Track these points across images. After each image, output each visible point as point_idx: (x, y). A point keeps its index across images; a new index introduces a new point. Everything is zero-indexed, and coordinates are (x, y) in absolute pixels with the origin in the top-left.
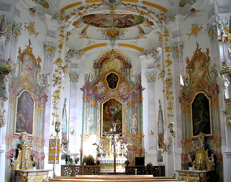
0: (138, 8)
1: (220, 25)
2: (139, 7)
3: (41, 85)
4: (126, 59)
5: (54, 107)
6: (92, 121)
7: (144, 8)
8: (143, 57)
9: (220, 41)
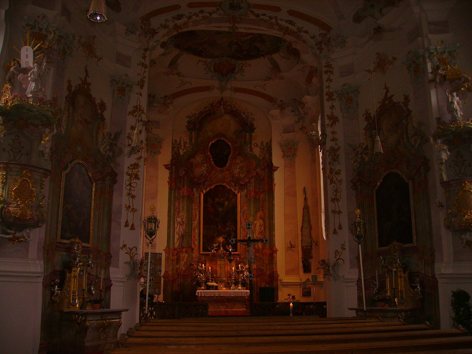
0: (279, 22)
1: (432, 53)
3: (106, 152)
4: (244, 116)
5: (129, 194)
6: (184, 225)
7: (291, 23)
8: (276, 112)
9: (433, 81)
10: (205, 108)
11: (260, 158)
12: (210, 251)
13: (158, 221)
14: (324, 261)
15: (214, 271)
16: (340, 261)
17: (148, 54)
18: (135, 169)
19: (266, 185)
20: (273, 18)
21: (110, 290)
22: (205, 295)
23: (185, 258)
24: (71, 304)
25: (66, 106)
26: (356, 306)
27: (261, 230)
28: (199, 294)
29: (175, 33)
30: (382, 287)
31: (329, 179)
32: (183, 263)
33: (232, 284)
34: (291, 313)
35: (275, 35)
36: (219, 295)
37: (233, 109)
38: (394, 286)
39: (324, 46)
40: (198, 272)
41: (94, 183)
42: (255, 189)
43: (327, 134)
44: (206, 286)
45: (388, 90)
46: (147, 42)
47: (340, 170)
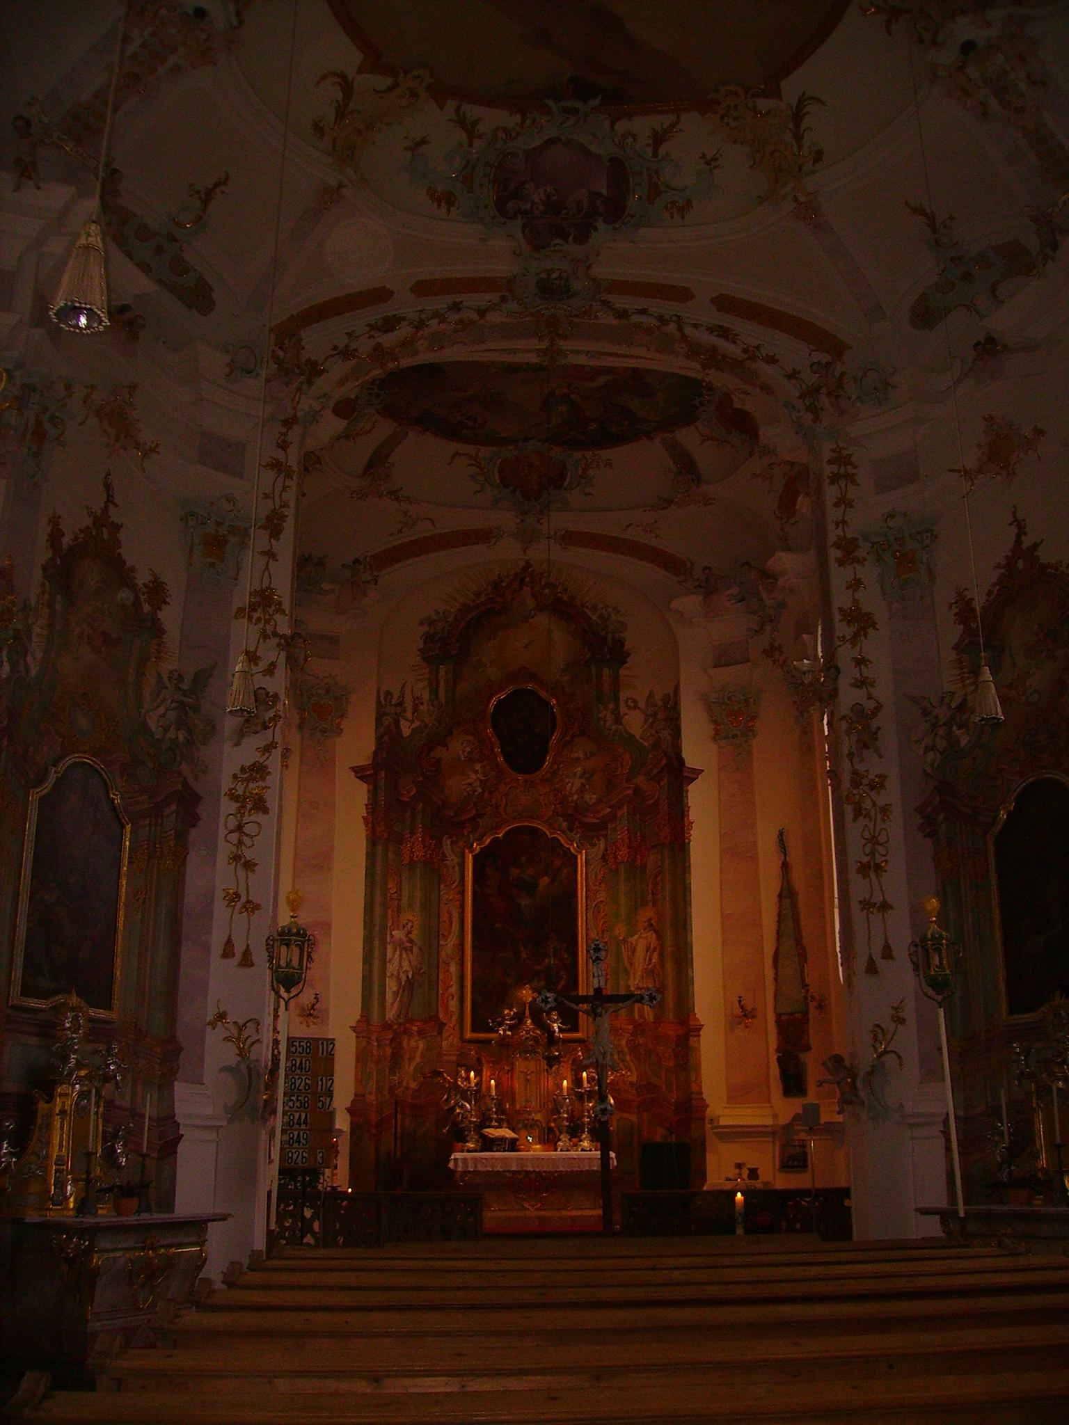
0: (688, 331)
2: (695, 326)
3: (166, 730)
5: (236, 858)
6: (415, 950)
7: (724, 333)
8: (690, 603)
10: (478, 595)
11: (646, 744)
12: (493, 1030)
13: (309, 940)
14: (838, 1060)
15: (506, 1093)
16: (890, 1060)
17: (294, 434)
18: (254, 779)
19: (664, 825)
20: (671, 321)
21: (176, 1152)
22: (476, 1166)
23: (419, 1053)
24: (51, 1199)
25: (43, 593)
26: (941, 1202)
27: (650, 963)
28: (460, 1164)
29: (377, 372)
30: (1022, 1141)
31: (848, 804)
32: (412, 1068)
33: (561, 1133)
34: (740, 1226)
35: (680, 372)
36: (519, 1169)
37: (560, 595)
38: (1058, 1137)
39: (825, 401)
40: (456, 1095)
41: (128, 825)
42: (629, 838)
43: (839, 665)
44: (480, 1140)
45: (1023, 526)
46: (293, 400)
47: (882, 777)
